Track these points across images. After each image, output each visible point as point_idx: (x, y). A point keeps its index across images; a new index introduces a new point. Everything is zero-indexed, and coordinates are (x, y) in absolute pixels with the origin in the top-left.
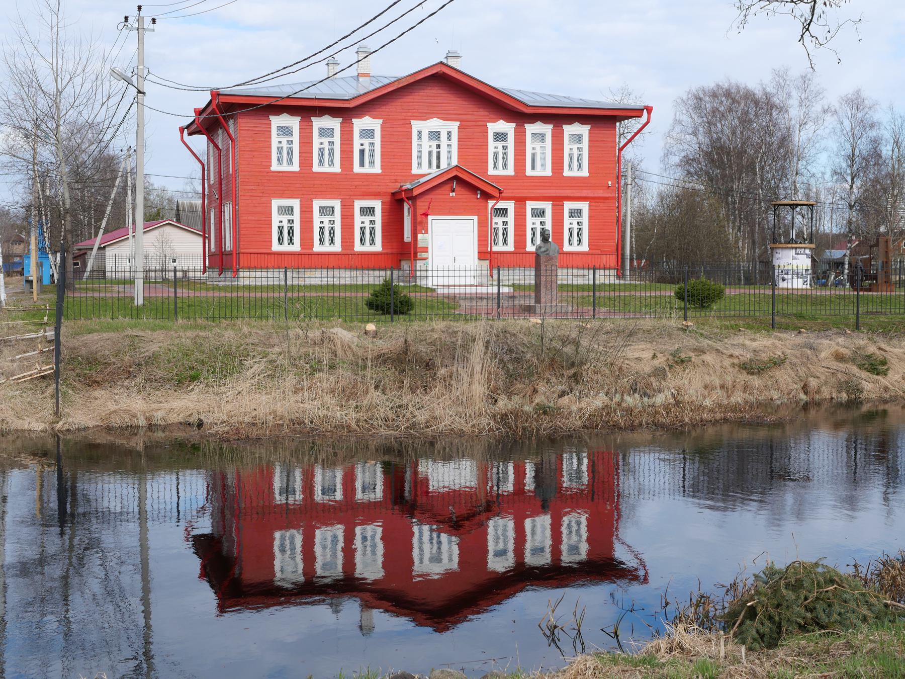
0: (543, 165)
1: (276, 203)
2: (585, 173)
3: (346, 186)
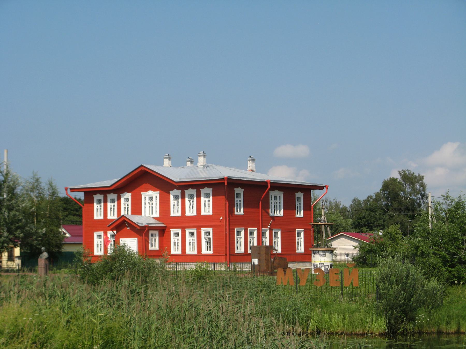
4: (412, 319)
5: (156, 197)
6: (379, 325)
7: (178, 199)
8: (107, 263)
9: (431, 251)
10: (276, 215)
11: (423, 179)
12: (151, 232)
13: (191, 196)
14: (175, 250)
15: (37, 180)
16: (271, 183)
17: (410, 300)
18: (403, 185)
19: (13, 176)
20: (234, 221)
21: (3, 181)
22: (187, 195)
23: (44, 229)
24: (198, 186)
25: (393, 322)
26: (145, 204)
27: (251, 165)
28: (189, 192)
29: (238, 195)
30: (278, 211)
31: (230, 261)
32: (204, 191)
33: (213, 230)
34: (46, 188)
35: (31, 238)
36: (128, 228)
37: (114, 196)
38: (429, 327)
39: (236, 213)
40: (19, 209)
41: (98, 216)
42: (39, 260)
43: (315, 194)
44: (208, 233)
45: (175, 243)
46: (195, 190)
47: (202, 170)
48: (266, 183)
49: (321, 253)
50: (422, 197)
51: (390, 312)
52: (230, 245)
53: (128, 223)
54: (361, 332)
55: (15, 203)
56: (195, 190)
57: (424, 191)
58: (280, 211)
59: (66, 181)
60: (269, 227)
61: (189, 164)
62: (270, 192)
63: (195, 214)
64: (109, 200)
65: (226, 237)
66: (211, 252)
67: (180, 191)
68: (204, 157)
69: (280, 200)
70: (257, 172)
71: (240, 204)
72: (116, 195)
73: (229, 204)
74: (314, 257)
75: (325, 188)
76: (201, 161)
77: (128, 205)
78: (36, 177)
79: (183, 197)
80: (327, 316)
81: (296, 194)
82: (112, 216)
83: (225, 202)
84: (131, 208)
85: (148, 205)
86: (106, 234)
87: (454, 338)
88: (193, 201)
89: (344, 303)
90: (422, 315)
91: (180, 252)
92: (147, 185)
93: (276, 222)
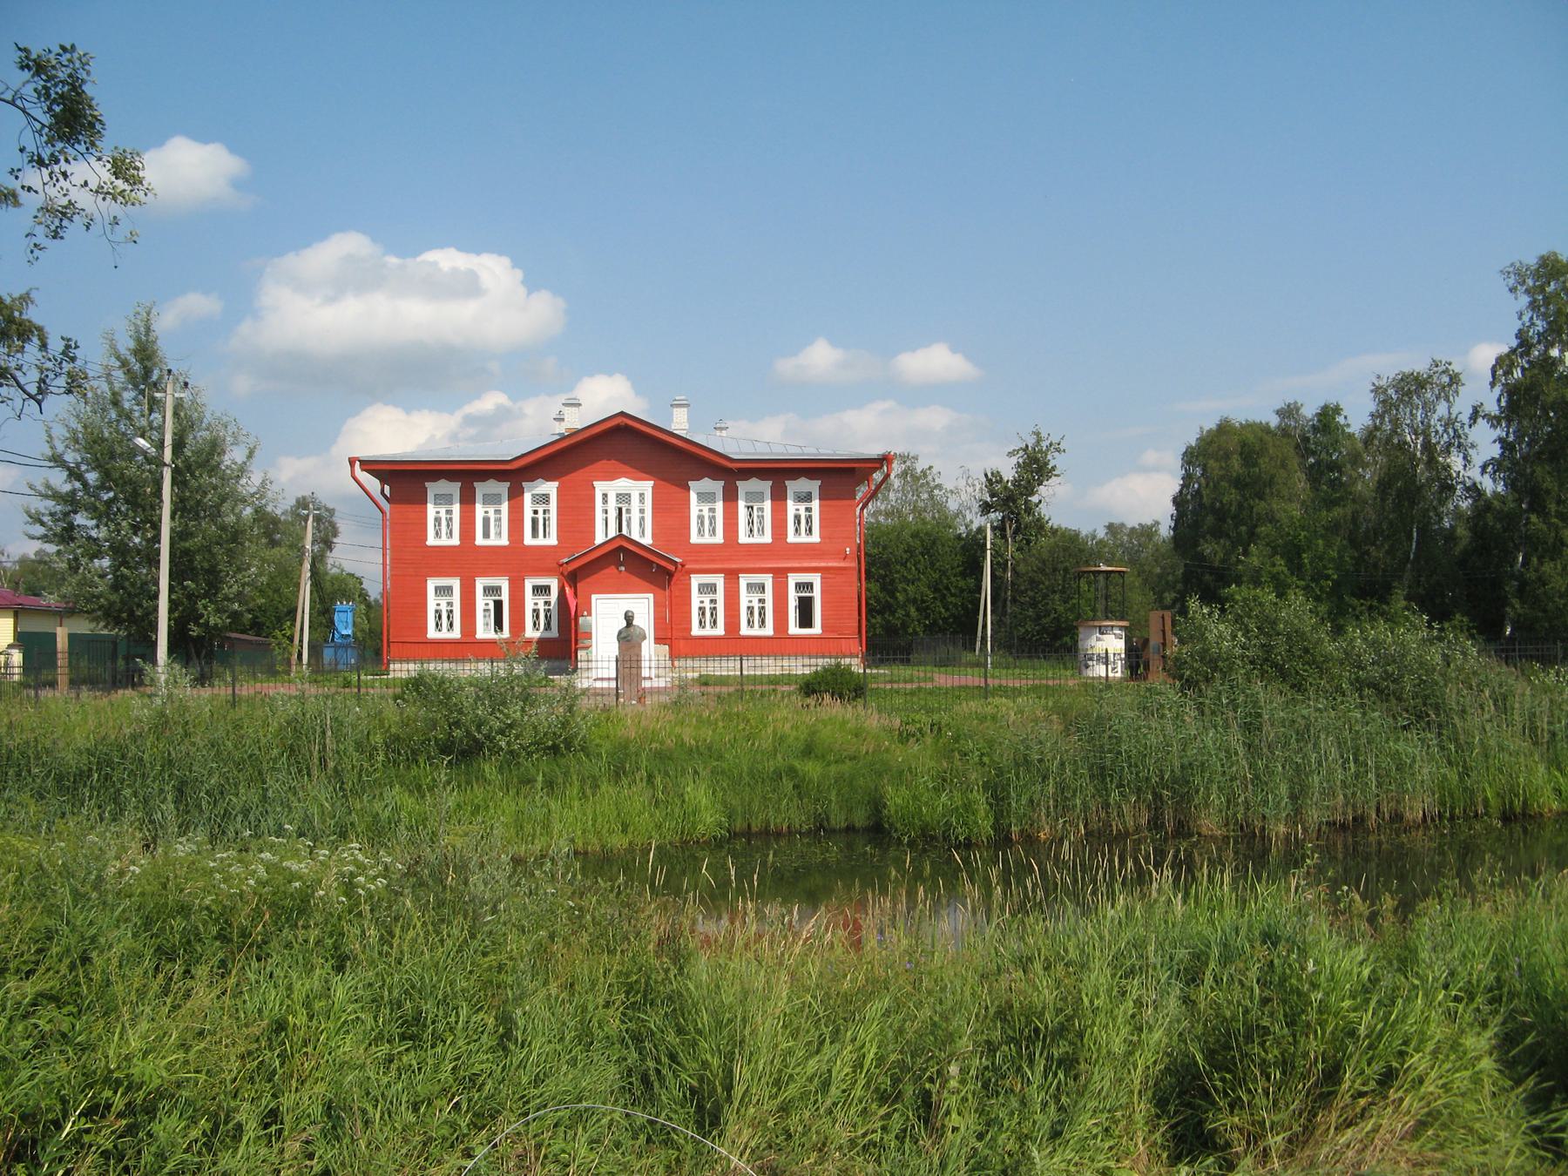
0: (500, 534)
1: (431, 584)
2: (815, 538)
3: (516, 561)
24: (778, 474)
92: (613, 464)
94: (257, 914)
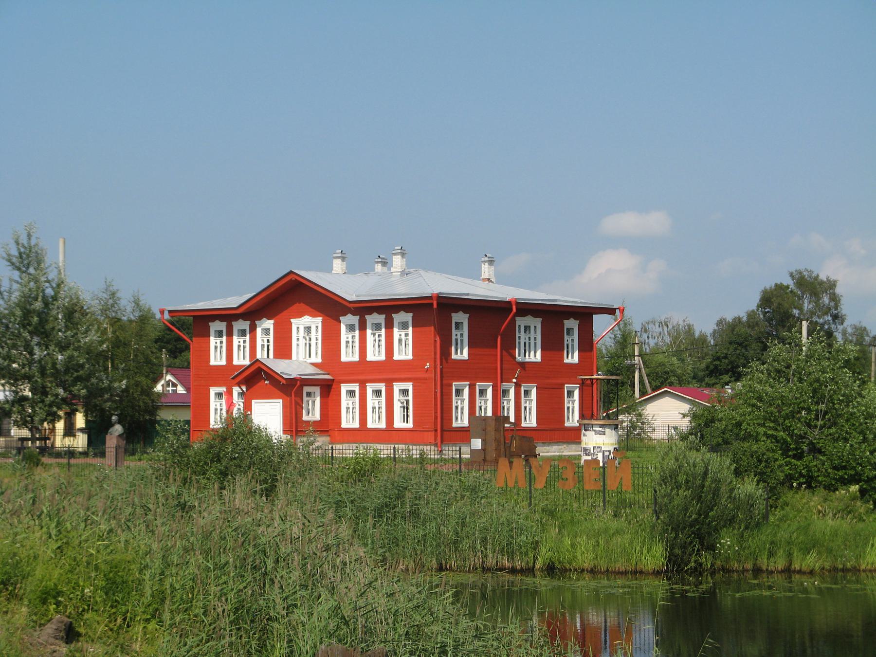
4: (712, 548)
5: (317, 327)
6: (654, 557)
7: (354, 331)
8: (211, 447)
9: (761, 430)
10: (527, 359)
11: (835, 285)
12: (306, 389)
13: (377, 327)
14: (349, 420)
15: (113, 294)
16: (517, 303)
17: (707, 516)
18: (798, 297)
19: (70, 289)
20: (449, 371)
21: (52, 297)
22: (369, 325)
23: (124, 382)
24: (388, 308)
25: (677, 551)
26: (298, 339)
27: (486, 270)
28: (373, 319)
29: (458, 325)
30: (532, 353)
31: (442, 442)
32: (400, 317)
33: (413, 386)
34: (129, 309)
35: (101, 396)
36: (267, 382)
37: (245, 325)
38: (739, 561)
39: (454, 357)
40: (80, 346)
41: (217, 359)
42: (108, 437)
43: (598, 320)
44: (405, 392)
45: (348, 408)
46: (384, 316)
47: (399, 280)
48: (509, 303)
49: (598, 429)
50: (834, 320)
51: (673, 535)
52: (442, 413)
53: (265, 372)
54: (623, 569)
55: (73, 336)
56: (384, 316)
57: (836, 309)
58: (535, 353)
59: (166, 296)
60: (514, 380)
61: (379, 268)
62: (517, 318)
63: (383, 357)
64: (235, 332)
65: (436, 398)
66: (410, 425)
67: (357, 317)
68: (403, 257)
69: (535, 332)
70: (497, 283)
71: (462, 341)
72: (248, 323)
73: (441, 341)
74: (584, 435)
75: (617, 311)
76: (398, 262)
77: (268, 341)
78: (111, 288)
79: (363, 327)
80: (568, 542)
81: (565, 322)
82: (241, 360)
83: (435, 336)
84: (274, 346)
85: (302, 342)
86: (230, 393)
87: (779, 579)
88: (379, 336)
89: (604, 519)
90: (726, 541)
91: (356, 425)
93: (527, 372)
94: (667, 566)
